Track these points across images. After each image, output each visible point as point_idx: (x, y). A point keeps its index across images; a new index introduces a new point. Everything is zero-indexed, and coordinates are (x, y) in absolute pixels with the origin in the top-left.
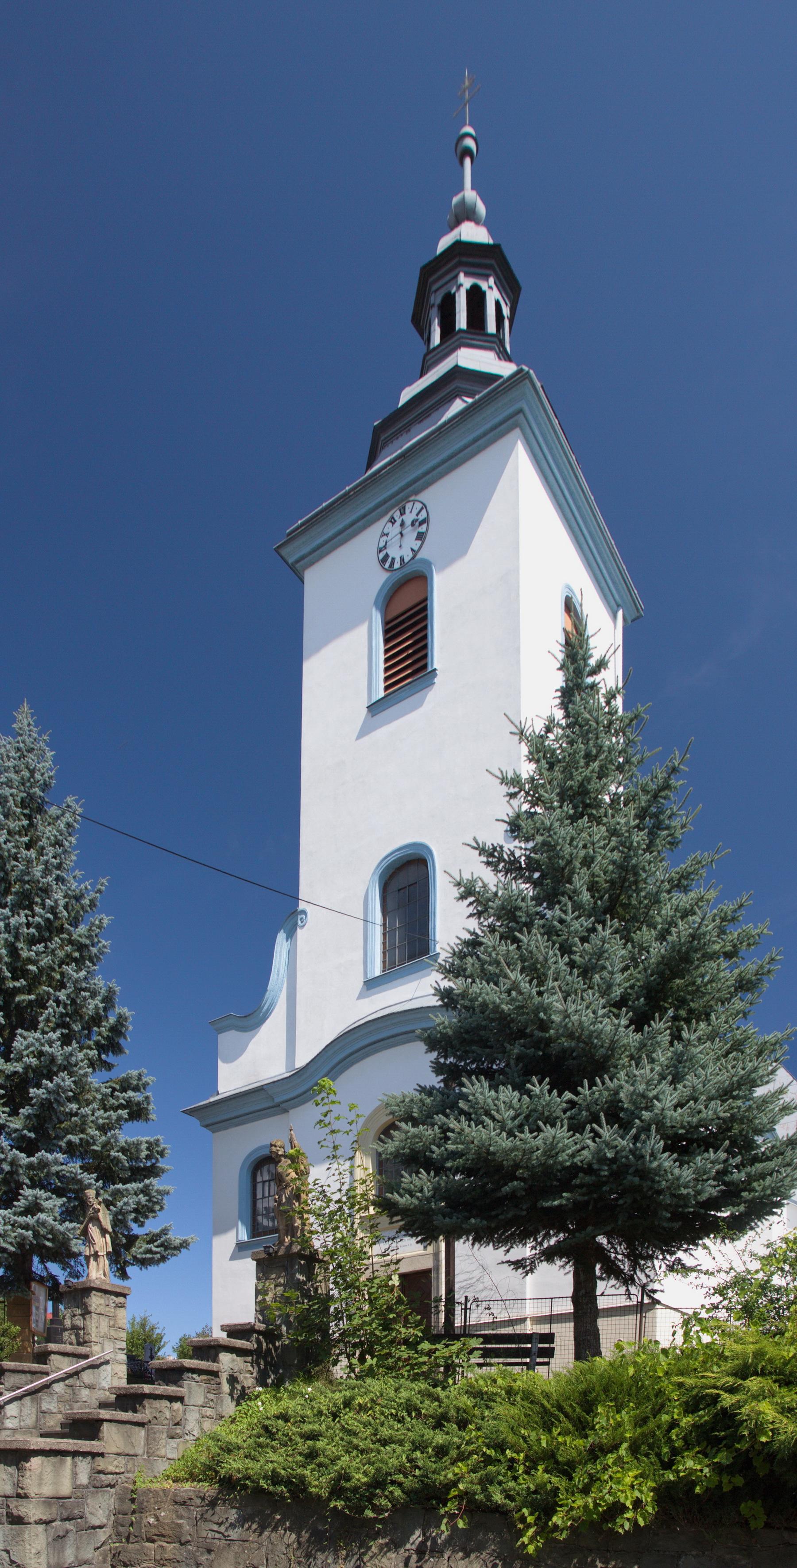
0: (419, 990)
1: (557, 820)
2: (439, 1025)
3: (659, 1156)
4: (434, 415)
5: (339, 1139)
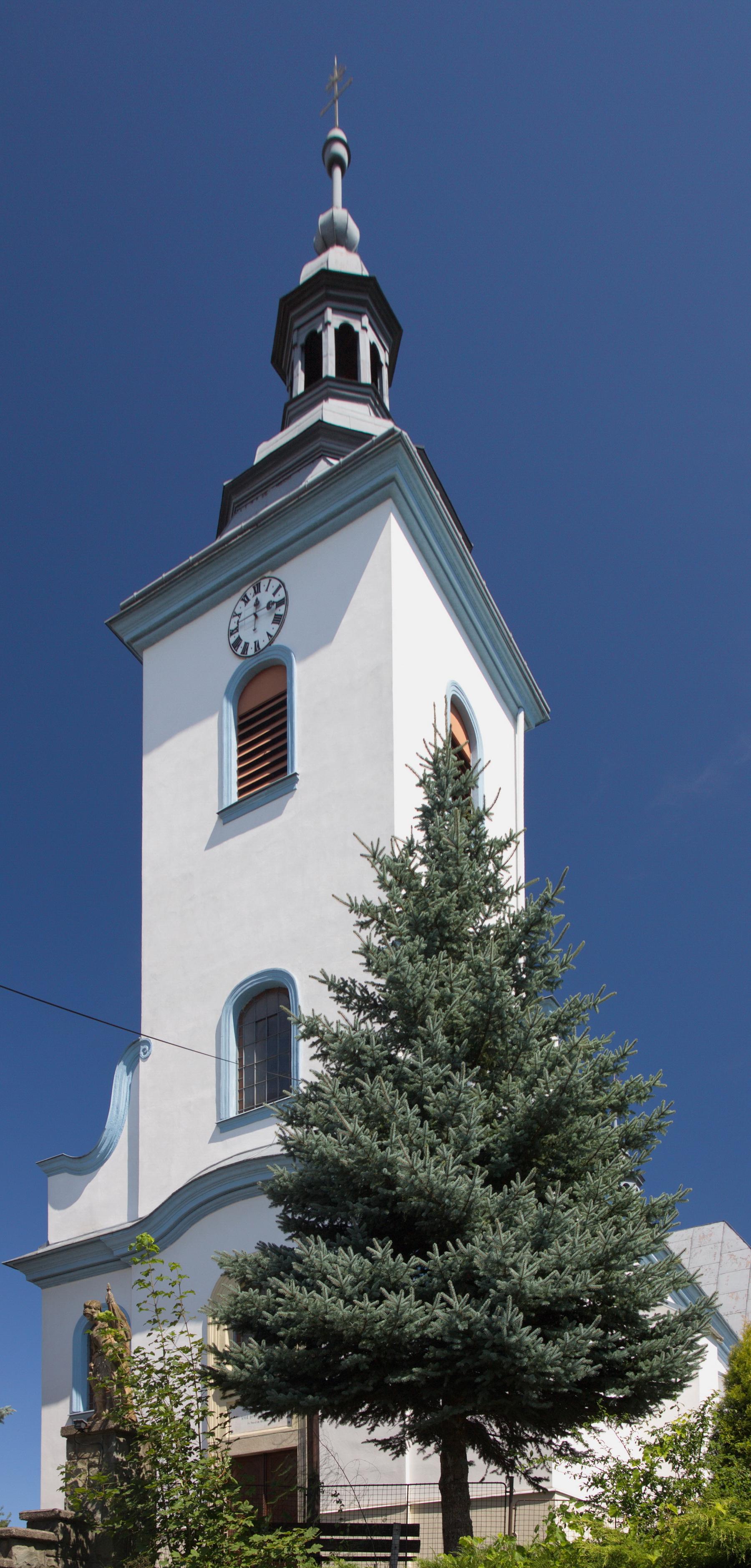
0: (264, 1139)
1: (405, 955)
2: (278, 1177)
3: (519, 1330)
4: (295, 477)
5: (162, 1302)
